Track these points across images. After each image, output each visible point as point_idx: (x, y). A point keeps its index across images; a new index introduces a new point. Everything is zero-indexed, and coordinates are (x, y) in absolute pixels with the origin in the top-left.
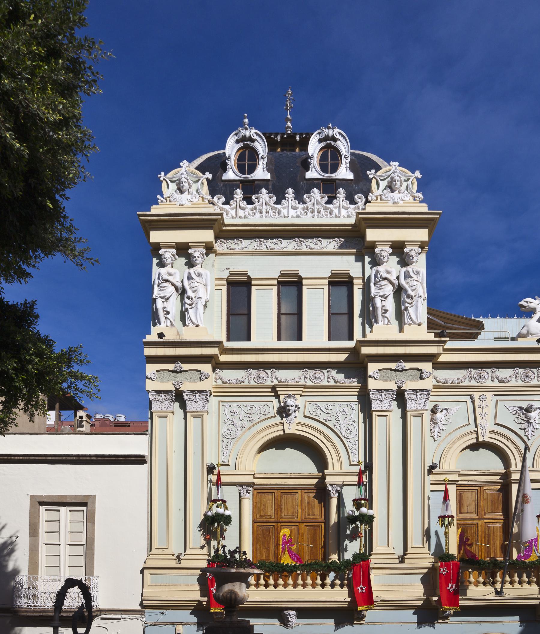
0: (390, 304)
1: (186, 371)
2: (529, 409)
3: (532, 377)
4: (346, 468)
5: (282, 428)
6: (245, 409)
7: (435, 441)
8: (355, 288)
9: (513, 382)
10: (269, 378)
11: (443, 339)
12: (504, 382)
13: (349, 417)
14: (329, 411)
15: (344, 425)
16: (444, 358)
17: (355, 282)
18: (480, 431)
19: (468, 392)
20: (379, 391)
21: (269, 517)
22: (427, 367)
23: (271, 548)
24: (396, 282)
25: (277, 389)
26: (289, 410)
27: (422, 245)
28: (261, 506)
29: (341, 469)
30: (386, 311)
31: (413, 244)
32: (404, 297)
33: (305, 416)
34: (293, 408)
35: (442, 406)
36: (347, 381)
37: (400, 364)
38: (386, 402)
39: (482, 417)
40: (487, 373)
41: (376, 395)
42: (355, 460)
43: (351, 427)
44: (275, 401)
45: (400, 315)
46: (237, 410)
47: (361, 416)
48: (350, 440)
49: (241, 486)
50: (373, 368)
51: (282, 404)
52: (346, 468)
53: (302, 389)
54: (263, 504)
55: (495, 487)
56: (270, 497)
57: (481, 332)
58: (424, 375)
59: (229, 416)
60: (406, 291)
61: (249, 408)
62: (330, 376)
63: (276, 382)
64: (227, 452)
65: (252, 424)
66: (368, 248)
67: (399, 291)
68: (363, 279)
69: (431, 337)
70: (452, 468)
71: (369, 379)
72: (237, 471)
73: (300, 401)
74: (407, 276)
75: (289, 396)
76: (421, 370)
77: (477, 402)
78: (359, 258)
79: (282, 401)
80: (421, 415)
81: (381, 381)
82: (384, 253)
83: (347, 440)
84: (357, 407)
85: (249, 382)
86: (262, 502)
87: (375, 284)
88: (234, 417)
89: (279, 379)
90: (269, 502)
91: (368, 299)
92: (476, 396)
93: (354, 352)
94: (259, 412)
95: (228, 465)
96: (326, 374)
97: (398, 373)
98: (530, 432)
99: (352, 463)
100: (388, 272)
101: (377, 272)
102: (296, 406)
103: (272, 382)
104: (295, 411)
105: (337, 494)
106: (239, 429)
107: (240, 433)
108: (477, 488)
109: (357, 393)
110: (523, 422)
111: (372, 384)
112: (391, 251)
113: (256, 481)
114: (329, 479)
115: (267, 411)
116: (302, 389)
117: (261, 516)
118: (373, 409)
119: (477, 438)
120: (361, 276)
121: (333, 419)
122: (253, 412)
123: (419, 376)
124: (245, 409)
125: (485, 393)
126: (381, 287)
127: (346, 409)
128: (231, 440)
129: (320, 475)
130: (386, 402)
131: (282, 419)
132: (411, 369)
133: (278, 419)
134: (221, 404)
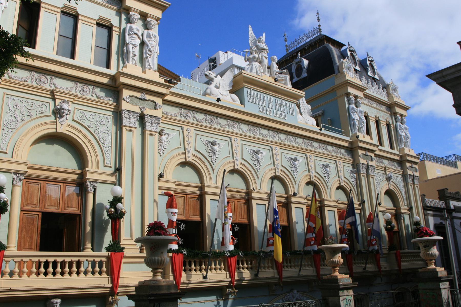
0: (137, 51)
1: (146, 100)
2: (213, 144)
3: (88, 92)
4: (102, 169)
5: (55, 126)
6: (26, 105)
7: (161, 156)
8: (114, 33)
9: (204, 124)
10: (48, 83)
11: (171, 85)
12: (199, 122)
13: (105, 127)
14: (92, 120)
15: (102, 133)
16: (168, 98)
17: (114, 29)
18: (276, 169)
19: (180, 124)
20: (129, 111)
21: (34, 206)
22: (159, 101)
23: (34, 237)
24: (141, 38)
25: (55, 93)
26: (64, 113)
27: (158, 19)
28: (28, 194)
29: (98, 168)
30: (135, 55)
31: (153, 17)
32: (145, 49)
33: (73, 120)
34: (66, 112)
35: (166, 131)
36: (106, 99)
37: (143, 95)
38: (132, 120)
39: (189, 144)
40: (190, 113)
41: (127, 114)
42: (108, 162)
43: (106, 135)
44: (52, 103)
45: (142, 60)
46: (19, 104)
47: (114, 128)
48: (105, 145)
49: (16, 174)
50: (126, 93)
51: (59, 107)
52: (102, 169)
53: (74, 98)
54: (30, 193)
55: (195, 196)
56: (36, 186)
57: (177, 83)
58: (157, 107)
59: (11, 108)
60: (148, 46)
61: (30, 105)
62: (94, 92)
63: (53, 87)
64: (6, 140)
65: (30, 119)
66: (124, 9)
67: (143, 44)
68: (120, 29)
69: (162, 81)
70: (24, 160)
71: (123, 101)
72: (13, 159)
73: (71, 107)
74: (149, 36)
75: (65, 101)
76: (155, 103)
77: (233, 142)
78: (119, 13)
79: (57, 104)
80: (132, 131)
81: (130, 105)
82: (135, 17)
83: (104, 145)
84: (111, 120)
85: (32, 82)
86: (30, 191)
87: (128, 35)
88: (16, 109)
89: (56, 85)
90: (36, 191)
91: (123, 43)
92: (185, 128)
93: (113, 78)
94: (37, 109)
95: (6, 153)
96: (91, 90)
97: (141, 101)
98: (214, 159)
99: (106, 165)
100: (138, 30)
101: (131, 28)
102: (69, 111)
103: (51, 86)
104: (67, 115)
105: (93, 190)
106: (19, 121)
107: (19, 124)
108: (184, 195)
109: (112, 110)
110: (210, 152)
111: (125, 106)
112: (139, 17)
113: (30, 171)
114: (88, 176)
115: (44, 109)
116: (74, 98)
117: (28, 204)
118: (146, 129)
119: (340, 184)
120: (118, 26)
121: (94, 126)
122: (32, 108)
123: (154, 106)
124: (26, 105)
125: (190, 128)
126: (133, 38)
127: (104, 120)
128: (11, 130)
129: (80, 172)
130: (132, 120)
131: (56, 119)
132: (150, 100)
133: (52, 119)
134: (6, 96)
